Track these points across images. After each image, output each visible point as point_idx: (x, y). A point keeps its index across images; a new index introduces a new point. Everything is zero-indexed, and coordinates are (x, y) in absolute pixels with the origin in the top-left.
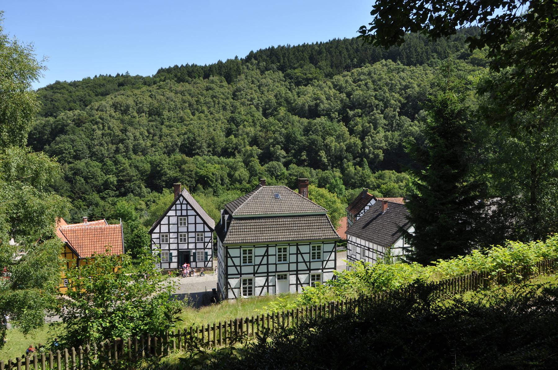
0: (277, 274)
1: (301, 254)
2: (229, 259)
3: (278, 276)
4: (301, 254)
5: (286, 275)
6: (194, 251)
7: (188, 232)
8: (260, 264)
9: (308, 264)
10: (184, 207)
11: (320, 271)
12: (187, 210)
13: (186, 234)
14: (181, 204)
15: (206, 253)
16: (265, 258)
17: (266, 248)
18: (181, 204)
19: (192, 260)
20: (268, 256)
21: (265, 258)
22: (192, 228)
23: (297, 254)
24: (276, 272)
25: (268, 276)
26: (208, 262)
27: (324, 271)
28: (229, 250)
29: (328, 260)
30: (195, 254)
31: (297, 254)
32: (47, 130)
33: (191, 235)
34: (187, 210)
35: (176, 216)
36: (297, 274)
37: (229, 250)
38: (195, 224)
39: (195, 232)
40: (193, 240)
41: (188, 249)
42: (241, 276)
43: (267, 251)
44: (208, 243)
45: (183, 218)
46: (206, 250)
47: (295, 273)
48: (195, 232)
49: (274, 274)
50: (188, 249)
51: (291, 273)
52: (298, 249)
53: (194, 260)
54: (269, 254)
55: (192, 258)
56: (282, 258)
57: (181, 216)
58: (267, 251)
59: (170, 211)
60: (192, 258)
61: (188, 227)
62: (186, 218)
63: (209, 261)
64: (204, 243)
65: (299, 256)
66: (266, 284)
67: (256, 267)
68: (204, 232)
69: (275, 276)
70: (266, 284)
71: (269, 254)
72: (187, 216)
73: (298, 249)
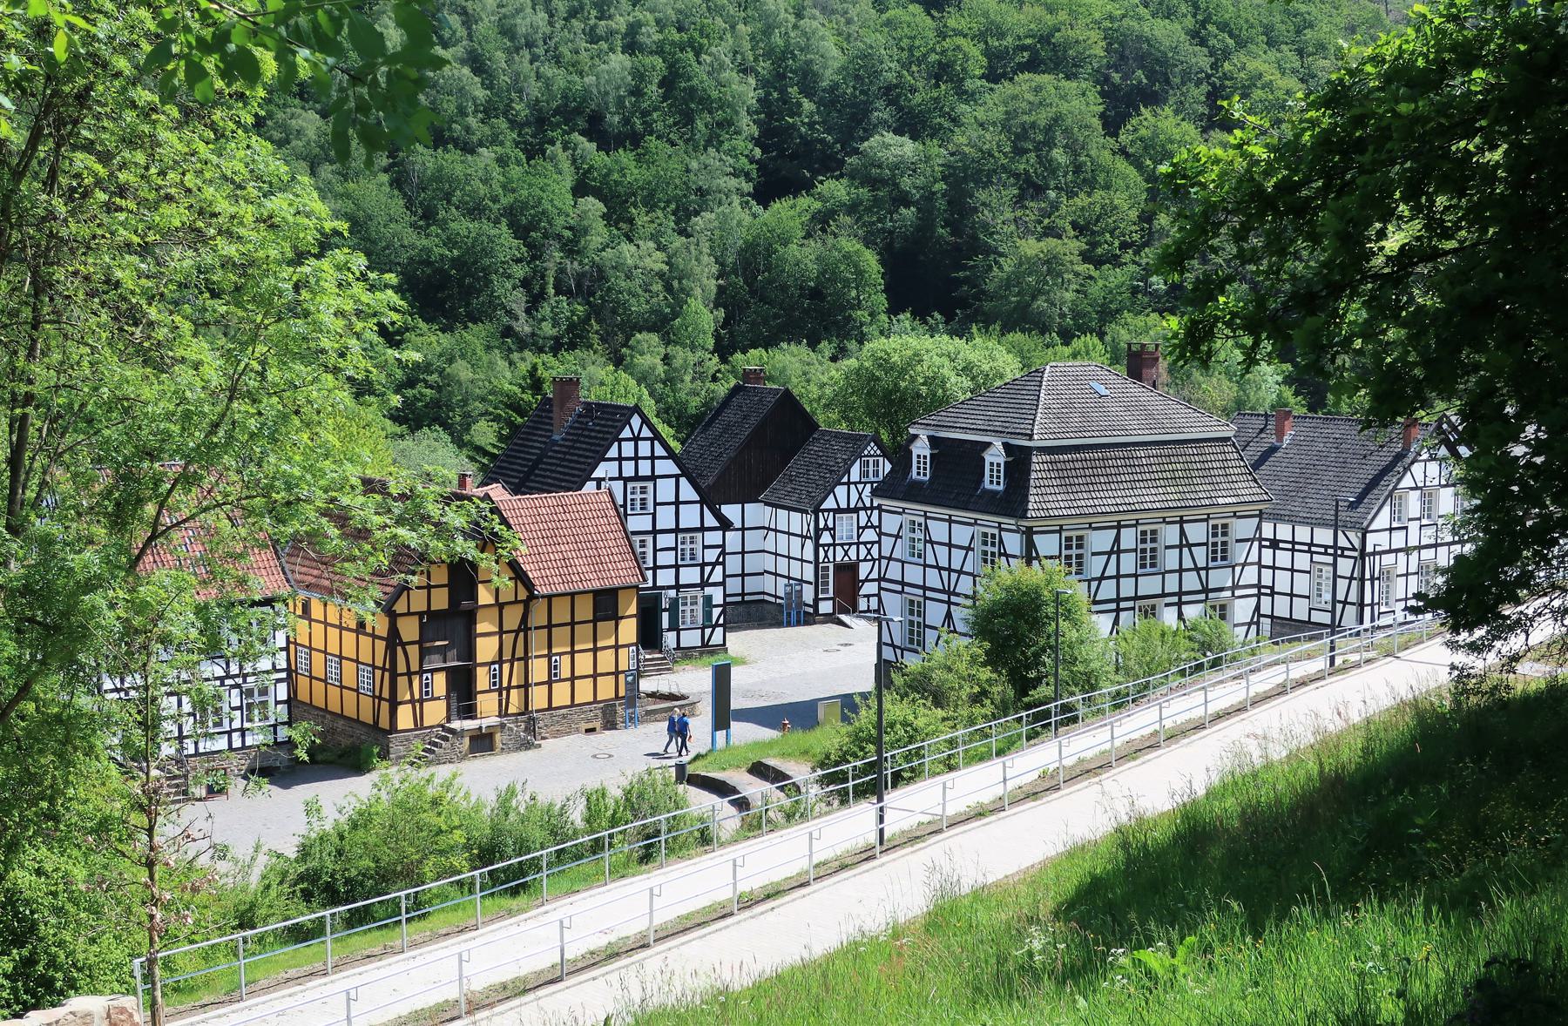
0: (1139, 603)
5: (1153, 607)
6: (672, 593)
7: (655, 532)
8: (1102, 578)
9: (1203, 573)
10: (644, 449)
11: (1228, 593)
12: (653, 458)
13: (649, 539)
14: (636, 439)
15: (708, 600)
18: (636, 439)
19: (665, 625)
20: (1119, 552)
22: (666, 518)
26: (714, 627)
27: (1238, 593)
29: (1244, 565)
30: (674, 603)
32: (1000, 268)
33: (666, 540)
34: (653, 458)
35: (620, 477)
38: (677, 503)
39: (677, 530)
40: (666, 558)
41: (655, 587)
43: (1117, 539)
44: (714, 565)
45: (638, 485)
46: (708, 591)
48: (677, 530)
49: (1130, 604)
50: (655, 587)
52: (1182, 533)
53: (674, 627)
55: (665, 616)
56: (1148, 560)
57: (637, 478)
58: (1117, 539)
59: (602, 464)
60: (665, 616)
61: (654, 515)
62: (650, 485)
63: (717, 625)
64: (703, 565)
65: (1185, 550)
67: (1094, 584)
68: (702, 529)
72: (653, 478)
73: (1182, 533)
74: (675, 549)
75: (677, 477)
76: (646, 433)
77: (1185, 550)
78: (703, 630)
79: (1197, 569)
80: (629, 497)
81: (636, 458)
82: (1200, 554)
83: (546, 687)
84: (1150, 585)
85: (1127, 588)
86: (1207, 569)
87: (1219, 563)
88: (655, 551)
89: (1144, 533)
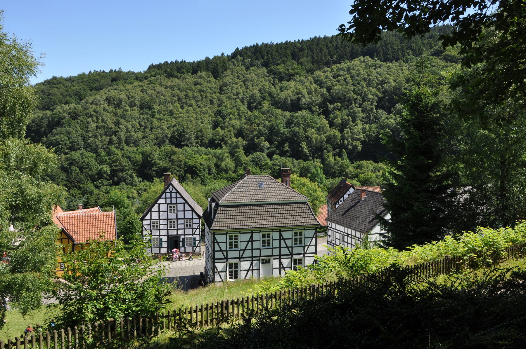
0: (261, 258)
1: (284, 239)
2: (216, 245)
3: (262, 260)
4: (284, 239)
5: (269, 259)
6: (183, 237)
7: (177, 219)
8: (245, 249)
9: (290, 249)
10: (174, 195)
11: (302, 256)
12: (176, 198)
13: (176, 221)
14: (171, 192)
15: (194, 239)
16: (250, 243)
17: (251, 234)
18: (171, 192)
19: (181, 245)
20: (252, 241)
21: (250, 243)
22: (181, 215)
23: (280, 240)
24: (260, 256)
25: (252, 261)
26: (197, 247)
27: (306, 255)
28: (216, 236)
29: (309, 246)
30: (183, 239)
31: (280, 240)
32: (44, 123)
33: (180, 221)
34: (176, 198)
35: (166, 203)
36: (280, 259)
37: (216, 236)
38: (184, 211)
39: (184, 219)
40: (182, 226)
41: (177, 234)
42: (227, 261)
43: (252, 237)
44: (196, 229)
45: (172, 205)
46: (194, 236)
47: (278, 257)
48: (184, 219)
49: (258, 258)
50: (177, 234)
51: (274, 257)
52: (281, 235)
53: (183, 246)
54: (254, 239)
55: (181, 243)
56: (266, 243)
57: (171, 203)
58: (252, 237)
59: (160, 199)
60: (181, 243)
61: (177, 214)
62: (176, 205)
63: (197, 246)
64: (193, 229)
65: (282, 241)
66: (251, 268)
67: (242, 252)
68: (192, 218)
69: (259, 260)
70: (251, 268)
71: (254, 239)
72: (176, 203)
73: (281, 235)
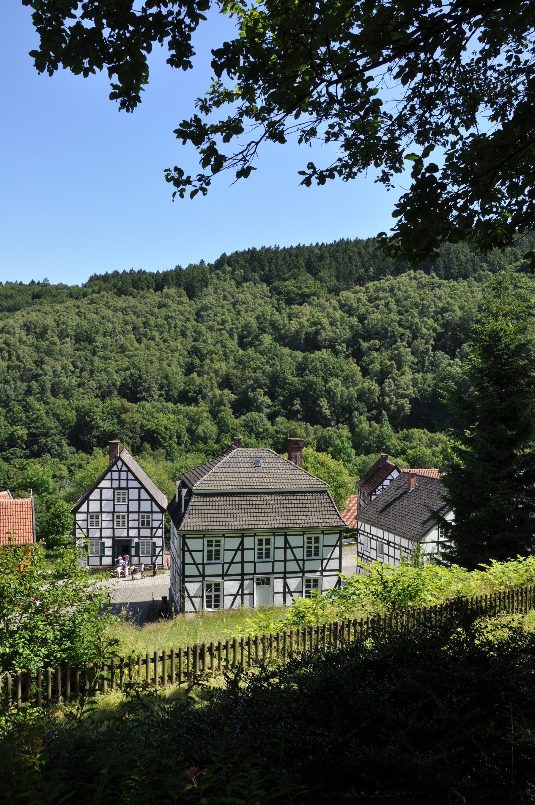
1: (291, 548)
3: (258, 579)
4: (291, 548)
5: (268, 579)
6: (136, 540)
7: (128, 512)
8: (232, 562)
10: (123, 475)
11: (318, 574)
14: (120, 471)
15: (154, 544)
16: (239, 553)
17: (241, 539)
18: (120, 471)
20: (243, 550)
21: (239, 553)
23: (285, 548)
24: (255, 573)
26: (157, 556)
27: (324, 574)
30: (137, 544)
31: (285, 548)
33: (133, 516)
34: (127, 480)
36: (285, 578)
37: (187, 540)
38: (139, 500)
39: (139, 512)
41: (128, 537)
43: (242, 543)
44: (157, 528)
46: (154, 540)
49: (251, 577)
50: (128, 537)
51: (276, 576)
52: (286, 541)
53: (137, 554)
56: (264, 554)
57: (119, 488)
58: (242, 543)
59: (103, 481)
61: (128, 505)
62: (126, 491)
63: (159, 555)
64: (152, 528)
65: (289, 551)
68: (152, 512)
69: (253, 579)
72: (128, 488)
73: (286, 541)
74: (87, 520)
75: (139, 489)
76: (124, 468)
77: (289, 551)
78: (152, 557)
79: (296, 560)
80: (116, 496)
81: (119, 480)
82: (299, 553)
83: (245, 560)
84: (264, 568)
85: (249, 568)
86: (303, 560)
87: (313, 557)
88: (128, 521)
89: (260, 540)
